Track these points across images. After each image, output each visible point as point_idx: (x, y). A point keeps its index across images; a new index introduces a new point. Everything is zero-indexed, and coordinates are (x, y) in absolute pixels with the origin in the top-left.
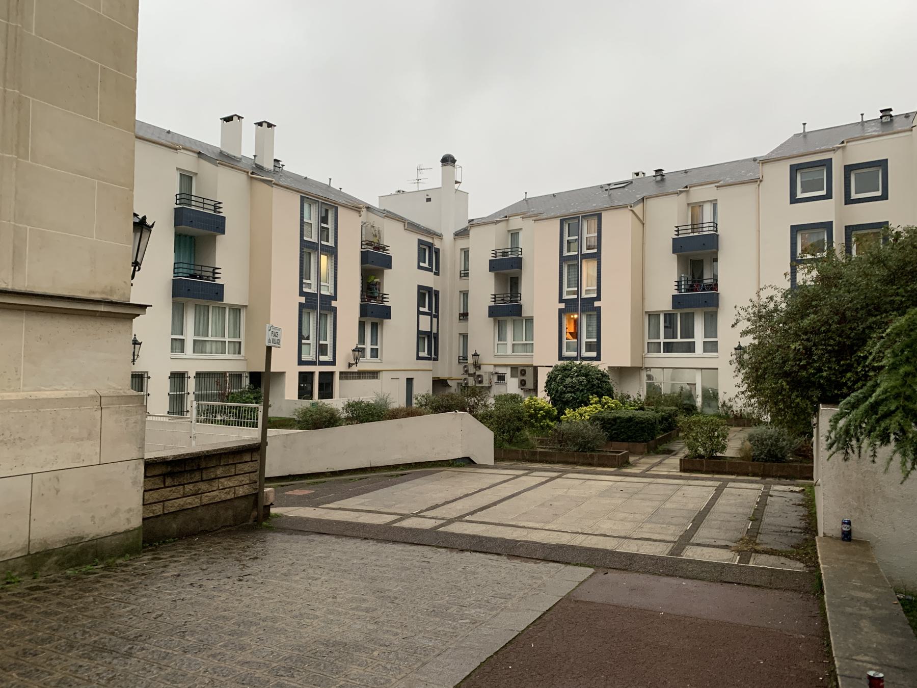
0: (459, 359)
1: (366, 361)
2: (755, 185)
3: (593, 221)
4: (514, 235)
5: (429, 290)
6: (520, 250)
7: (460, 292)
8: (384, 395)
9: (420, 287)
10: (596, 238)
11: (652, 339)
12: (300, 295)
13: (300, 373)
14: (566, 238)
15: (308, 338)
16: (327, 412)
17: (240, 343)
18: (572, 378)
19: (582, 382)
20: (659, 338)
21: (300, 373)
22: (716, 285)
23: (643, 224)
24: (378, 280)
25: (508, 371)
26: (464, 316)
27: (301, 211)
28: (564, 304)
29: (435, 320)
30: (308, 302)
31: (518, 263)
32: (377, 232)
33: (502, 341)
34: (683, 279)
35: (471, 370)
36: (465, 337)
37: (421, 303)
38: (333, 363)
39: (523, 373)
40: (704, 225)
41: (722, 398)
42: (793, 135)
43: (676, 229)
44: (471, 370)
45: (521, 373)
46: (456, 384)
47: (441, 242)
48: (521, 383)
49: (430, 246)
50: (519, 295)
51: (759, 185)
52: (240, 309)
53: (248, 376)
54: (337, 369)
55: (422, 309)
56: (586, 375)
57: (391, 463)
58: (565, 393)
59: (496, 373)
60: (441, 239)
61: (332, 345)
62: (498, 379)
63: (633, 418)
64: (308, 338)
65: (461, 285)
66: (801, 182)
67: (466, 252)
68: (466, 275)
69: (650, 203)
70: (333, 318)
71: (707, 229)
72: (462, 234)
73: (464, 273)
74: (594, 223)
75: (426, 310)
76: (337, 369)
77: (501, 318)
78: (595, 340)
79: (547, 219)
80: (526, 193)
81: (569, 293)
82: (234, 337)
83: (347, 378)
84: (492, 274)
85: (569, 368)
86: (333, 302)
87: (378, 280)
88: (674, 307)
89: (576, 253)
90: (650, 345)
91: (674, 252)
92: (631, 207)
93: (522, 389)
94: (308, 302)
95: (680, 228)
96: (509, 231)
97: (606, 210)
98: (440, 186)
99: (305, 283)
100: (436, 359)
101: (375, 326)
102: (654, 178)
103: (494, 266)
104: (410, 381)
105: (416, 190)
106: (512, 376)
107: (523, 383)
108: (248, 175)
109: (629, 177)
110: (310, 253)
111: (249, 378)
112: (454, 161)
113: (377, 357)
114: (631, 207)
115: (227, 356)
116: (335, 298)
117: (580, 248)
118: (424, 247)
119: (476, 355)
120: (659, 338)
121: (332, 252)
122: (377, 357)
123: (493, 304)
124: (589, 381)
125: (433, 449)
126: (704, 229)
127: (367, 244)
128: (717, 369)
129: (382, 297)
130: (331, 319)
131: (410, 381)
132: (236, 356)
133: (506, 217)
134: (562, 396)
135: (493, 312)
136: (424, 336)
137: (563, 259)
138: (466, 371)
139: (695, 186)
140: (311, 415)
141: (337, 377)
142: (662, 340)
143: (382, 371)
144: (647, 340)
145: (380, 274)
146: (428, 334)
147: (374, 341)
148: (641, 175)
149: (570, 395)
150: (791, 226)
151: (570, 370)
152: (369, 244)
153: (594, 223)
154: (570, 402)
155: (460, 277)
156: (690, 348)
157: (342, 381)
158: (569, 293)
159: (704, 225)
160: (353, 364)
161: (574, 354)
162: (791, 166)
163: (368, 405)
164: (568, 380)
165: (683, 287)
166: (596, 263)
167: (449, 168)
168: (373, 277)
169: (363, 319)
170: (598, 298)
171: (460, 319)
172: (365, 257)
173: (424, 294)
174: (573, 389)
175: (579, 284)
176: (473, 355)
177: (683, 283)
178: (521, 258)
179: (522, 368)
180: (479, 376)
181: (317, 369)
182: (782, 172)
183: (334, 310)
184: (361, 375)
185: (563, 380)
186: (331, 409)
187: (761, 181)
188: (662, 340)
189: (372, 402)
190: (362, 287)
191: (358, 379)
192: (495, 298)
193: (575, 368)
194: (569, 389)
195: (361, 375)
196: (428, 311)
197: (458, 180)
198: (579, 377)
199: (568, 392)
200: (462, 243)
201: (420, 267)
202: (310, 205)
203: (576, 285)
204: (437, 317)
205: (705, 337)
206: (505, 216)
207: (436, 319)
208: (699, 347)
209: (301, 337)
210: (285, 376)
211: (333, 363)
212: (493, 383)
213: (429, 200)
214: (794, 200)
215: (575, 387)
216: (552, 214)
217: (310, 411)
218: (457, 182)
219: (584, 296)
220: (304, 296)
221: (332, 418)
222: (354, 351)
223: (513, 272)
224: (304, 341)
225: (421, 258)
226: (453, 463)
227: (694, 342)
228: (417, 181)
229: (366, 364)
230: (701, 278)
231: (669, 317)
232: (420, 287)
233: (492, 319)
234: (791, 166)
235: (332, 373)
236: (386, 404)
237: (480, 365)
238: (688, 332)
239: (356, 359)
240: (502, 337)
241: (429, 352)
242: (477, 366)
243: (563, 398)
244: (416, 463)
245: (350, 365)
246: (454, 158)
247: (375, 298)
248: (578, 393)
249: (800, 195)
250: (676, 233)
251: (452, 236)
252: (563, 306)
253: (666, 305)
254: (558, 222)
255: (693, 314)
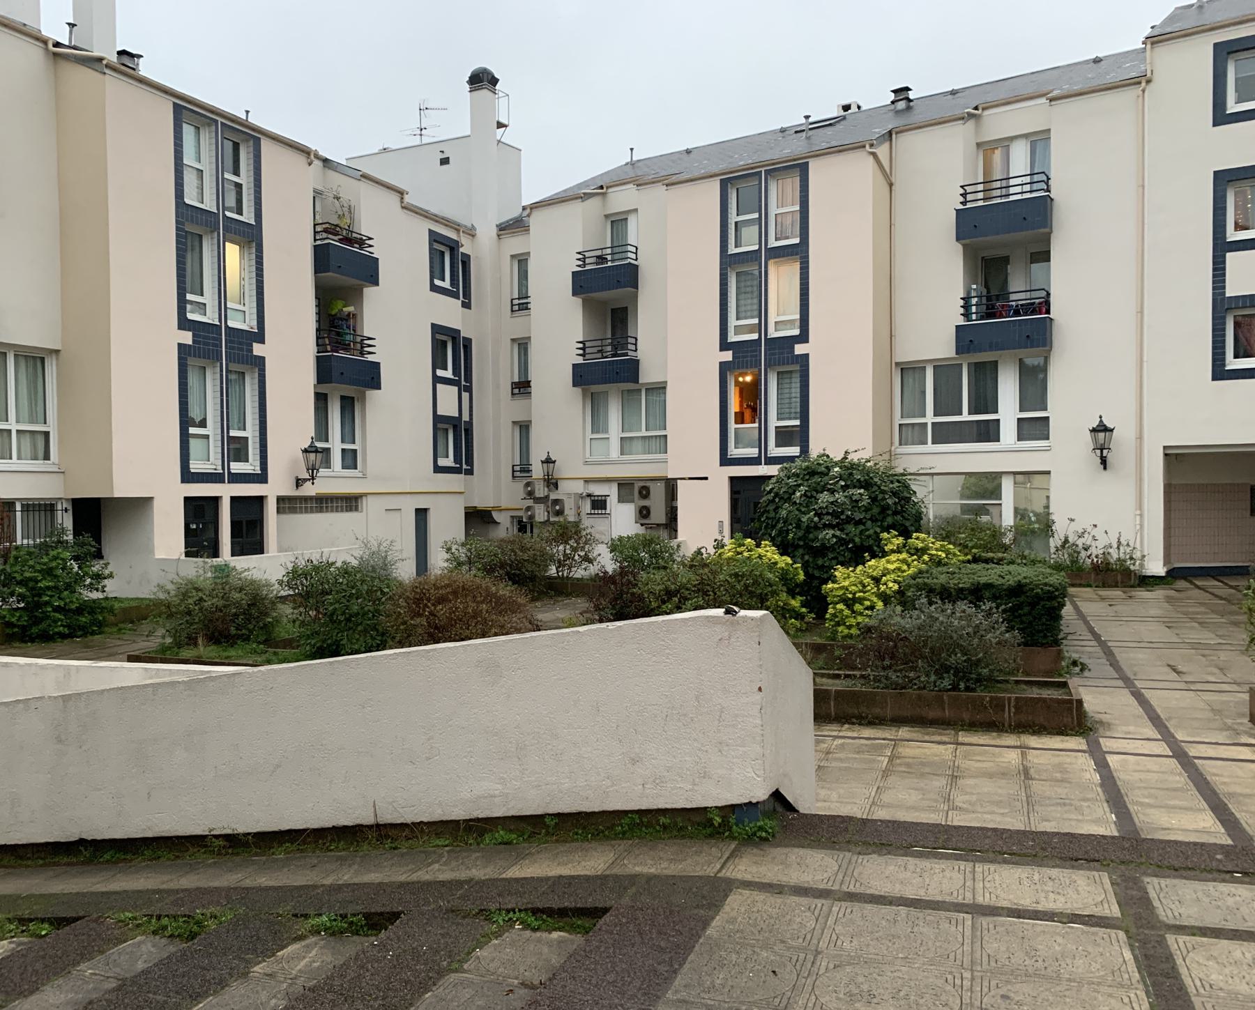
0: (513, 471)
1: (332, 474)
2: (1134, 92)
3: (789, 180)
4: (618, 223)
5: (454, 334)
6: (634, 249)
7: (513, 340)
8: (380, 545)
9: (436, 329)
10: (798, 216)
11: (909, 417)
12: (181, 327)
13: (187, 500)
14: (733, 218)
15: (203, 424)
16: (241, 590)
17: (47, 434)
18: (832, 492)
19: (857, 501)
20: (924, 416)
21: (187, 500)
22: (1047, 303)
23: (891, 185)
24: (351, 309)
25: (612, 492)
26: (522, 387)
27: (175, 137)
28: (730, 352)
29: (465, 395)
30: (199, 343)
31: (629, 276)
32: (346, 209)
33: (598, 432)
34: (973, 294)
35: (541, 491)
36: (524, 428)
37: (438, 361)
38: (262, 478)
39: (645, 493)
40: (1012, 182)
41: (1061, 528)
42: (1173, 9)
43: (962, 191)
44: (541, 491)
45: (640, 493)
46: (509, 520)
47: (472, 241)
48: (640, 512)
49: (453, 247)
50: (631, 340)
51: (1143, 91)
52: (43, 360)
53: (70, 508)
54: (271, 490)
55: (440, 373)
56: (867, 485)
57: (458, 813)
58: (816, 528)
59: (589, 495)
60: (473, 236)
61: (258, 440)
62: (593, 508)
63: (1026, 584)
64: (203, 424)
65: (516, 327)
66: (1237, 80)
67: (522, 261)
68: (524, 307)
69: (903, 141)
70: (256, 381)
71: (1018, 189)
72: (514, 226)
73: (519, 304)
74: (792, 184)
75: (448, 374)
76: (271, 490)
77: (595, 388)
78: (797, 422)
79: (692, 180)
80: (632, 149)
81: (739, 330)
82: (32, 422)
83: (293, 510)
84: (578, 301)
85: (823, 469)
86: (255, 345)
87: (351, 309)
88: (960, 349)
89: (756, 247)
90: (904, 428)
91: (958, 239)
92: (871, 145)
93: (642, 525)
94: (199, 343)
95: (969, 189)
96: (607, 216)
97: (817, 155)
98: (468, 133)
99: (191, 302)
100: (470, 472)
101: (348, 405)
102: (893, 107)
103: (582, 283)
104: (421, 514)
105: (418, 143)
106: (621, 500)
107: (644, 513)
108: (47, 49)
109: (835, 112)
110: (200, 237)
111: (70, 512)
112: (494, 81)
113: (356, 468)
114: (871, 145)
115: (14, 463)
116: (260, 337)
117: (763, 235)
118: (442, 248)
119: (548, 461)
120: (924, 416)
121: (251, 237)
122: (356, 468)
123: (580, 360)
124: (874, 499)
125: (634, 761)
126: (1012, 190)
127: (325, 231)
128: (1048, 473)
129: (362, 345)
130: (252, 384)
131: (421, 514)
132: (39, 465)
133: (602, 187)
134: (811, 536)
135: (581, 376)
136: (445, 426)
137: (728, 261)
138: (530, 494)
139: (997, 106)
140: (201, 599)
141: (271, 507)
142: (930, 418)
143: (366, 495)
144: (898, 420)
145: (355, 295)
146: (455, 423)
147: (348, 434)
148: (854, 109)
149: (831, 532)
150: (1215, 172)
151: (827, 474)
152: (332, 230)
153: (792, 184)
154: (832, 548)
155: (512, 311)
156: (989, 432)
157: (284, 517)
158: (739, 330)
159: (1012, 182)
160: (305, 480)
161: (753, 452)
162: (1216, 45)
163: (346, 571)
164: (824, 498)
165: (974, 309)
166: (797, 266)
167: (484, 94)
168: (340, 304)
169: (324, 389)
170: (803, 337)
171: (513, 394)
172: (322, 258)
173: (444, 344)
174: (838, 518)
175: (762, 312)
176: (543, 462)
177: (974, 301)
178: (637, 266)
179: (642, 484)
180: (556, 502)
181: (225, 492)
182: (1200, 55)
183: (260, 363)
184: (324, 503)
185: (809, 497)
186: (253, 582)
187: (1148, 82)
188: (930, 418)
189: (355, 563)
190: (318, 321)
191: (317, 512)
192: (583, 349)
193: (836, 469)
194: (827, 519)
195: (324, 503)
196: (452, 377)
197: (506, 122)
198: (851, 491)
199: (826, 526)
200: (515, 244)
201: (434, 288)
202: (197, 128)
203: (756, 313)
204: (469, 389)
205: (1021, 410)
206: (601, 188)
207: (467, 394)
208: (1008, 431)
209: (185, 421)
210: (152, 508)
211: (262, 478)
212: (583, 514)
213: (445, 161)
214: (1221, 117)
215: (842, 512)
216: (703, 171)
217: (198, 589)
218: (500, 125)
219: (773, 333)
220: (189, 330)
221: (253, 604)
222: (305, 451)
223: (614, 295)
224: (192, 430)
225: (436, 270)
226: (725, 824)
227: (998, 421)
228: (419, 132)
229: (333, 481)
230: (1004, 294)
231: (944, 371)
232: (436, 329)
233: (578, 390)
234: (1216, 45)
235: (260, 500)
236: (385, 566)
237: (557, 479)
238: (985, 400)
239: (312, 469)
240: (598, 423)
241: (457, 458)
242: (551, 482)
243: (813, 541)
244: (559, 815)
245: (299, 483)
246: (493, 77)
247: (346, 348)
248: (850, 528)
249: (1232, 107)
250: (962, 199)
251: (494, 231)
252: (728, 356)
253: (942, 346)
254: (714, 187)
255: (995, 365)
